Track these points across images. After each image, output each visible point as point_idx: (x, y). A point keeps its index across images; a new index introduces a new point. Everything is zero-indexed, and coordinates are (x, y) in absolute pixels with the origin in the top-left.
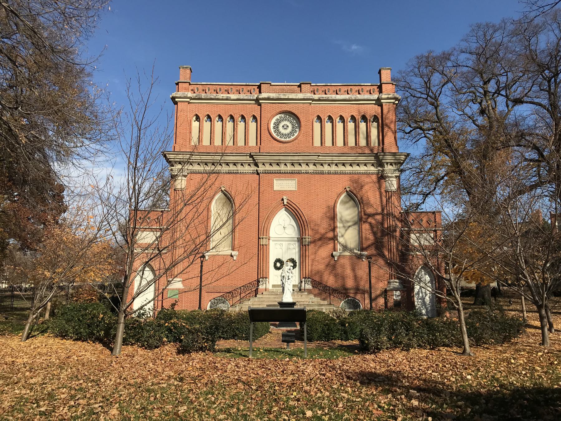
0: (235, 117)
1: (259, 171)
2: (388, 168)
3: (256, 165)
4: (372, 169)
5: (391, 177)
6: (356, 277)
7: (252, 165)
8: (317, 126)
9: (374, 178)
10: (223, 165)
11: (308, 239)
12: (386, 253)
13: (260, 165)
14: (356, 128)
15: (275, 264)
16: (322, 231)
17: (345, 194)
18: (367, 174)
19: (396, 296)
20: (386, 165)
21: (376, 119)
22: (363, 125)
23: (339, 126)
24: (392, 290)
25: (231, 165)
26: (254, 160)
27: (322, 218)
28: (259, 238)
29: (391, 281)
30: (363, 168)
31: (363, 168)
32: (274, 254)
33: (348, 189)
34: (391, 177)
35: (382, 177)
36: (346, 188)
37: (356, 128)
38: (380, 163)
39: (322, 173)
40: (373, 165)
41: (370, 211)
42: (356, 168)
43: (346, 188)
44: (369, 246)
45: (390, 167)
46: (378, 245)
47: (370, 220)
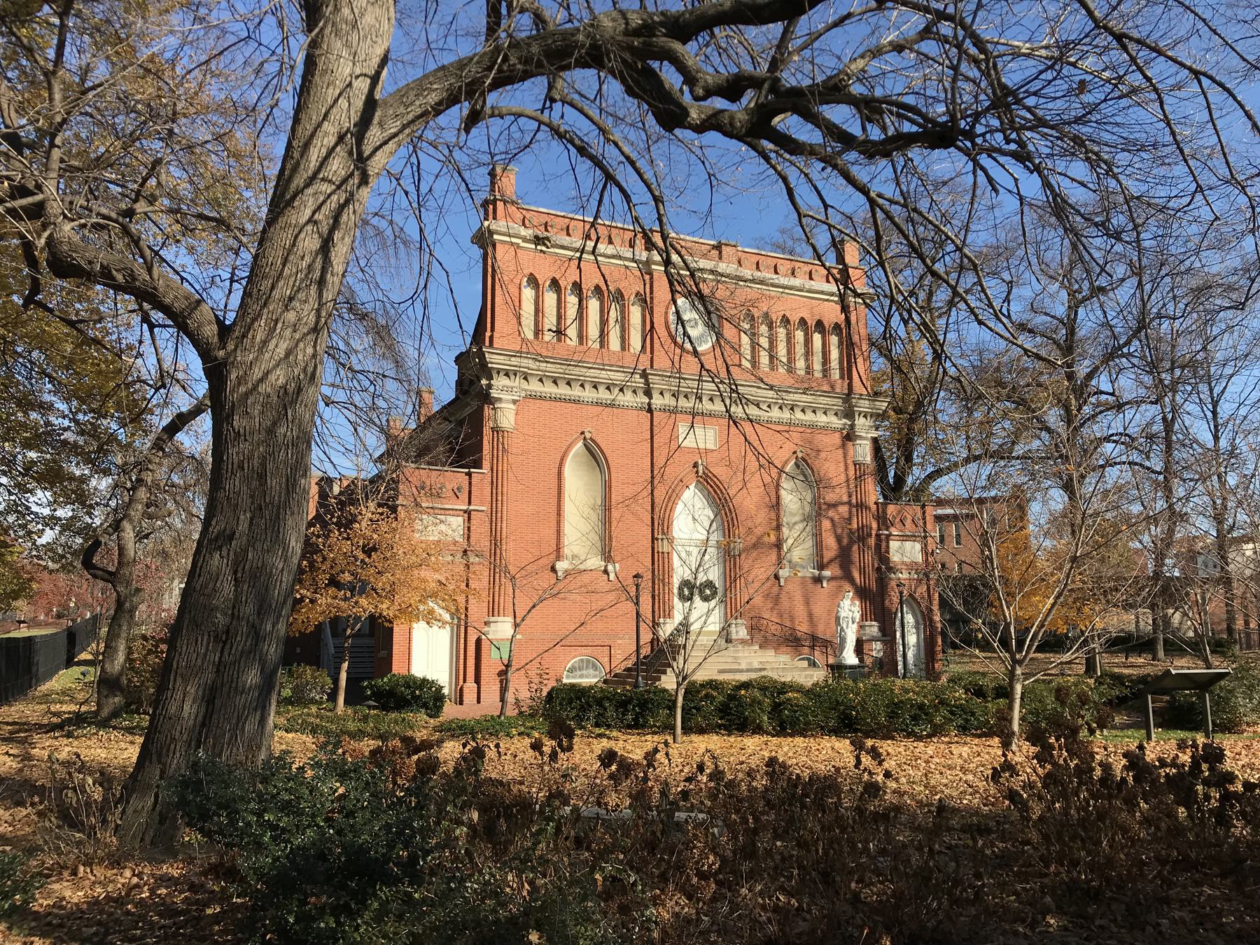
0: (562, 283)
1: (653, 407)
2: (860, 422)
3: (648, 393)
4: (837, 422)
5: (865, 438)
6: (810, 616)
7: (640, 393)
8: (528, 293)
9: (836, 439)
10: (587, 386)
11: (739, 545)
12: (856, 575)
13: (656, 395)
14: (808, 342)
15: (680, 589)
16: (759, 531)
17: (580, 444)
18: (825, 428)
19: (876, 650)
20: (495, 376)
21: (837, 327)
22: (817, 338)
23: (550, 299)
24: (870, 641)
25: (602, 389)
26: (647, 383)
27: (758, 508)
28: (653, 539)
29: (492, 619)
30: (822, 419)
31: (822, 419)
32: (680, 572)
33: (800, 455)
34: (865, 438)
35: (849, 436)
36: (583, 433)
37: (808, 342)
38: (849, 414)
39: (577, 401)
40: (836, 414)
41: (831, 497)
42: (809, 417)
43: (583, 433)
44: (831, 561)
45: (862, 420)
46: (844, 558)
47: (831, 513)
